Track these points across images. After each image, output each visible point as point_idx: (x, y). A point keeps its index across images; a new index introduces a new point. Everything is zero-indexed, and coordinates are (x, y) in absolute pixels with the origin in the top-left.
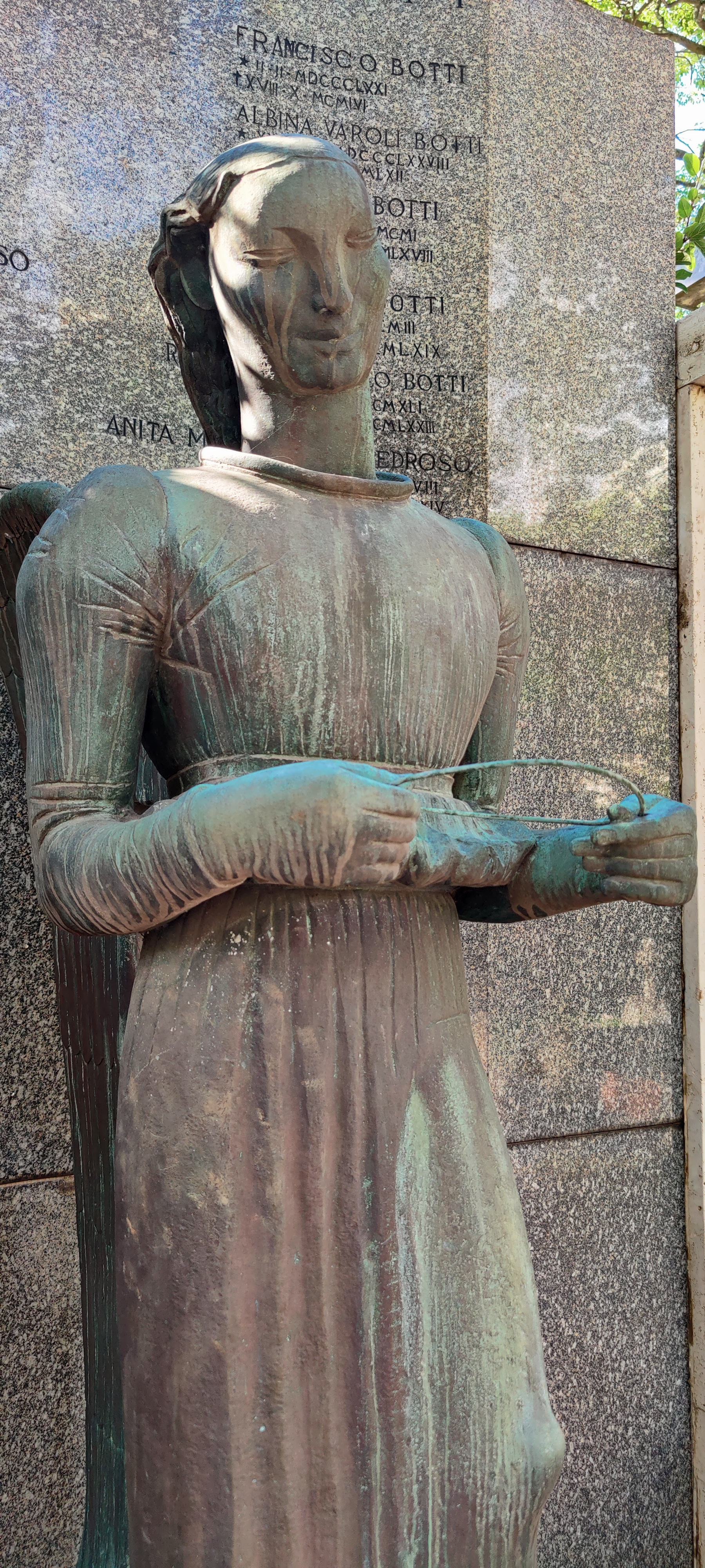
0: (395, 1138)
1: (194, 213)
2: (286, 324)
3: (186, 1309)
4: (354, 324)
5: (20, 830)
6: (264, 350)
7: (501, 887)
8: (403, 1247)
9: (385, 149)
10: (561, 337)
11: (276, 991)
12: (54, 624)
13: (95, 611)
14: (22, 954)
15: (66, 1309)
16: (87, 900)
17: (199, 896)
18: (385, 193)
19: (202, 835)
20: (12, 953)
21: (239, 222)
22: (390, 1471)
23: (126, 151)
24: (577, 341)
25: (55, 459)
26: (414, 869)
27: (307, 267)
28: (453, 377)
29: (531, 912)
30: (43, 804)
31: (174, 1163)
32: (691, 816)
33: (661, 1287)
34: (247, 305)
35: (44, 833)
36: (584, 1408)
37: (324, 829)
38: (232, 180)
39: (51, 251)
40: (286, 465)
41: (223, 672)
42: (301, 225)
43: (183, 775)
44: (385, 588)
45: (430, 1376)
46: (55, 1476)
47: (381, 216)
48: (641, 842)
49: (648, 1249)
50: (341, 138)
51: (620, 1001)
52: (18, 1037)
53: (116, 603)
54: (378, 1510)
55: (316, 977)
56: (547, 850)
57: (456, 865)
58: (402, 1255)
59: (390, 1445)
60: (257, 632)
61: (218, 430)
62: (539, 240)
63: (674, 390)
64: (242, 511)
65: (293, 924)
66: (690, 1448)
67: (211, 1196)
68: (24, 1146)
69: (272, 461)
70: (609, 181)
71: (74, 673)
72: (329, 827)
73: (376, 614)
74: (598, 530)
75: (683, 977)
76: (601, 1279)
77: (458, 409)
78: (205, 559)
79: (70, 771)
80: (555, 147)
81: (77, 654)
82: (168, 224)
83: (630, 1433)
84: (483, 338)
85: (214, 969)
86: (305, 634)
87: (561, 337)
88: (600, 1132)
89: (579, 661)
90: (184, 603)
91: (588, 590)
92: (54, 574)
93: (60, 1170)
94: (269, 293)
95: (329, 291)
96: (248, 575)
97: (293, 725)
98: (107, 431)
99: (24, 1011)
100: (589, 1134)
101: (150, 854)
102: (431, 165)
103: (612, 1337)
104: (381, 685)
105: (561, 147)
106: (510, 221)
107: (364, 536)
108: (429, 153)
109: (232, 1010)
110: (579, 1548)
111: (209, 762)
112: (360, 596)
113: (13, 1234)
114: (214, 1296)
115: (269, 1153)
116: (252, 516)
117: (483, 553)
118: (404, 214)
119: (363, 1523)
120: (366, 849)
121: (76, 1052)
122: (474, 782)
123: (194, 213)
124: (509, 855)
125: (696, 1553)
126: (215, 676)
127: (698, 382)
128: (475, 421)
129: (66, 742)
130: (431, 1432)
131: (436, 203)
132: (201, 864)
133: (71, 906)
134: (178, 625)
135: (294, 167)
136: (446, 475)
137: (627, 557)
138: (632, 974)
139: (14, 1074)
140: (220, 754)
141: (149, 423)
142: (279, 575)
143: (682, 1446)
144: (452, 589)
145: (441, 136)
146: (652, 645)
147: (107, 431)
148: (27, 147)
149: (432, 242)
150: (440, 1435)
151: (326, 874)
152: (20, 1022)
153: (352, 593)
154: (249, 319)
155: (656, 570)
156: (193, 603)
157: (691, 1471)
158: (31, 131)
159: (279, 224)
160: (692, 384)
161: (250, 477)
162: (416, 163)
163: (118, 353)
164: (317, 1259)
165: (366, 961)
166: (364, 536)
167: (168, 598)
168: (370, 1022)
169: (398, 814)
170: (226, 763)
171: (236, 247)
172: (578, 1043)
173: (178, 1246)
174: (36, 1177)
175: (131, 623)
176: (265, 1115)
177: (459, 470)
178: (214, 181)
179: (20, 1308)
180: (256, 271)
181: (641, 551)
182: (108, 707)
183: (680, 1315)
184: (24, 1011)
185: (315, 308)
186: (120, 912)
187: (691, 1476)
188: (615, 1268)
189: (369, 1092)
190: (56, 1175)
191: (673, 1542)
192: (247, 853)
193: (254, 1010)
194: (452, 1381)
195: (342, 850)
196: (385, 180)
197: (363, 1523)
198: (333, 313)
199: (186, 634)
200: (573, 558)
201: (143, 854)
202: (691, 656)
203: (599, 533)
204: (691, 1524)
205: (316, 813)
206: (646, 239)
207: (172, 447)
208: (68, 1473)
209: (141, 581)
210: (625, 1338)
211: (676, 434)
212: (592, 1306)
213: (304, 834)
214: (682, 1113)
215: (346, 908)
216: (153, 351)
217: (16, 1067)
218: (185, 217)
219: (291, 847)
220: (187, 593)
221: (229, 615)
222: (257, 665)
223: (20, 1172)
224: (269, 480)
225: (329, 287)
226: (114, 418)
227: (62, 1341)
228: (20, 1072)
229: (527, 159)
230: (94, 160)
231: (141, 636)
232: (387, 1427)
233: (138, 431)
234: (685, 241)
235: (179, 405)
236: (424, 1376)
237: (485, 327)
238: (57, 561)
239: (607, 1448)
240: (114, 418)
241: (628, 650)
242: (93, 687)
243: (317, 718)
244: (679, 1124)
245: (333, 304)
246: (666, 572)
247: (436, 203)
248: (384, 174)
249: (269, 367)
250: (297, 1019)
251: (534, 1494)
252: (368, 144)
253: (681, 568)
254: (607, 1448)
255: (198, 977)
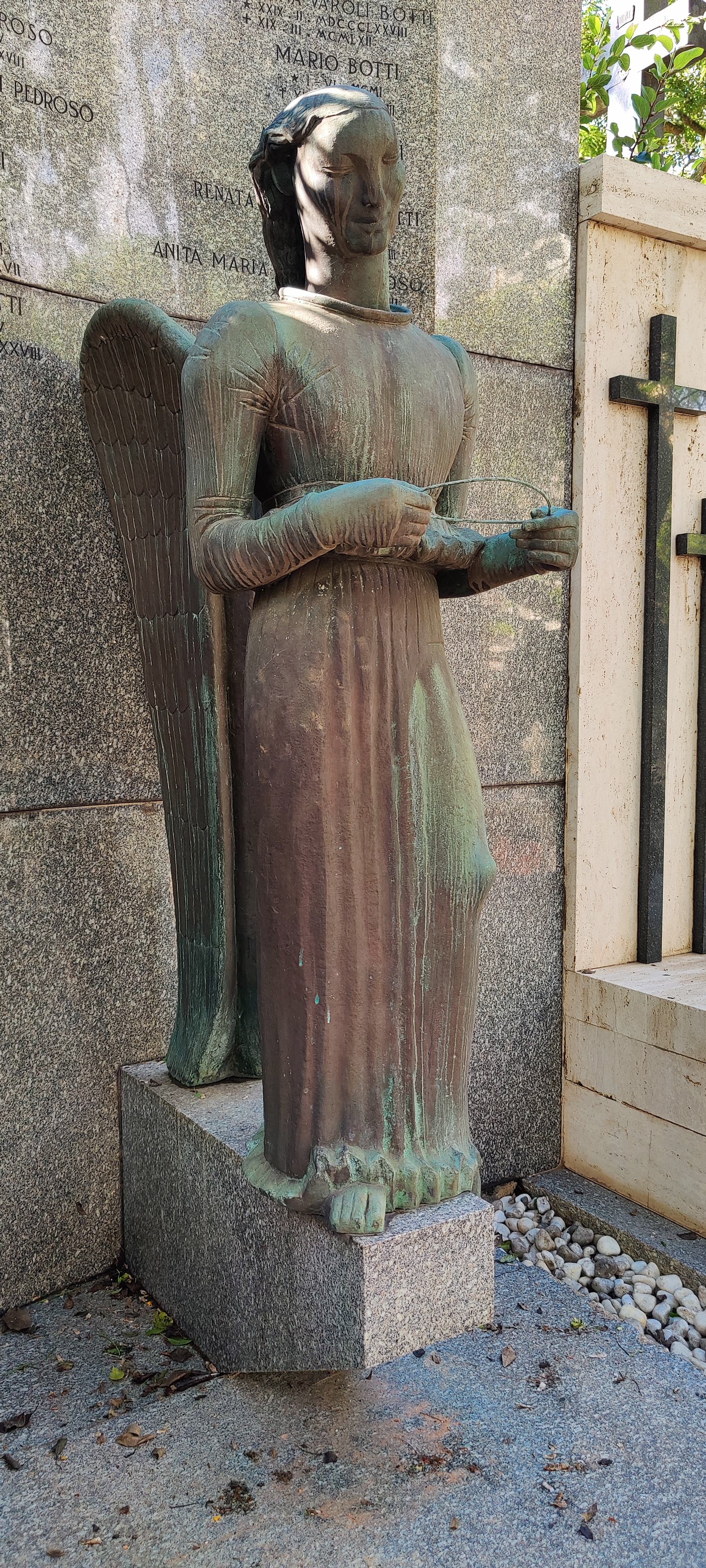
0: (408, 702)
1: (290, 138)
2: (345, 214)
3: (300, 786)
4: (385, 213)
5: (106, 558)
6: (330, 228)
7: (463, 570)
8: (412, 760)
9: (357, 18)
10: (491, 180)
11: (345, 616)
12: (213, 400)
13: (238, 392)
14: (112, 647)
15: (150, 889)
16: (238, 565)
17: (310, 555)
18: (358, 55)
19: (317, 519)
20: (105, 646)
21: (321, 149)
22: (406, 873)
23: (160, 20)
24: (503, 183)
25: (118, 276)
26: (420, 550)
27: (360, 177)
28: (410, 213)
29: (480, 586)
30: (204, 510)
31: (291, 709)
32: (577, 519)
33: (546, 892)
34: (323, 200)
35: (205, 528)
36: (492, 965)
37: (385, 514)
38: (316, 120)
39: (108, 105)
40: (342, 302)
41: (312, 431)
42: (358, 152)
43: (278, 497)
44: (402, 382)
45: (427, 827)
46: (148, 993)
47: (355, 75)
48: (549, 529)
49: (538, 866)
50: (323, 9)
51: (523, 695)
52: (112, 705)
53: (250, 388)
54: (400, 892)
55: (366, 609)
56: (492, 547)
57: (442, 550)
58: (412, 765)
59: (406, 860)
60: (333, 406)
61: (286, 274)
62: (475, 98)
63: (575, 224)
64: (319, 332)
65: (353, 579)
66: (561, 996)
67: (313, 725)
68: (119, 780)
69: (333, 299)
70: (530, 47)
71: (225, 430)
72: (388, 513)
73: (397, 397)
74: (515, 339)
75: (568, 679)
76: (505, 884)
77: (413, 240)
78: (301, 362)
79: (222, 490)
80: (488, 18)
81: (227, 418)
82: (268, 141)
83: (522, 983)
84: (433, 181)
85: (310, 604)
86: (359, 408)
87: (491, 180)
88: (507, 785)
89: (500, 441)
90: (287, 388)
91: (507, 387)
92: (214, 369)
93: (142, 798)
94: (338, 194)
95: (373, 193)
96: (326, 372)
97: (352, 463)
98: (154, 254)
99: (115, 687)
100: (499, 786)
101: (283, 532)
102: (393, 33)
103: (512, 922)
104: (400, 441)
105: (493, 19)
106: (454, 81)
107: (388, 348)
108: (391, 23)
109: (321, 626)
110: (487, 1053)
111: (299, 486)
112: (388, 386)
113: (114, 838)
114: (315, 777)
115: (344, 703)
116: (325, 335)
117: (454, 359)
118: (372, 74)
119: (392, 899)
120: (405, 526)
121: (162, 707)
122: (445, 508)
123: (290, 138)
124: (470, 549)
125: (564, 1063)
126: (306, 433)
127: (594, 218)
128: (426, 250)
129: (220, 472)
130: (427, 855)
131: (397, 65)
132: (315, 535)
133: (223, 570)
134: (283, 402)
135: (354, 115)
136: (404, 293)
137: (536, 361)
138: (532, 675)
139: (111, 730)
140: (307, 481)
141: (184, 248)
142: (343, 372)
143: (556, 995)
144: (438, 382)
145: (401, 9)
146: (554, 430)
147: (154, 254)
148: (88, 20)
149: (394, 98)
150: (432, 857)
151: (385, 539)
152: (112, 695)
153: (383, 384)
154: (323, 208)
155: (558, 372)
156: (294, 388)
157: (562, 1010)
158: (91, 7)
159: (345, 151)
160: (590, 219)
161: (319, 309)
162: (382, 30)
163: (159, 190)
164: (369, 764)
165: (392, 604)
166: (389, 348)
167: (278, 385)
168: (394, 637)
169: (422, 507)
170: (311, 486)
171: (318, 163)
172: (493, 723)
173: (295, 753)
174: (127, 801)
175: (257, 400)
176: (341, 683)
177: (414, 290)
178: (304, 120)
179: (121, 886)
180: (330, 179)
181: (546, 357)
182: (243, 451)
183: (558, 911)
184: (115, 687)
185: (364, 204)
186: (259, 570)
187: (562, 1014)
188: (515, 877)
189: (394, 676)
190: (140, 801)
191: (548, 1055)
192: (342, 528)
193: (334, 626)
194: (438, 830)
195: (394, 527)
196: (357, 44)
197: (392, 899)
198: (374, 207)
199: (288, 408)
200: (497, 361)
201: (277, 533)
202: (582, 440)
203: (516, 342)
204: (561, 1045)
205: (382, 505)
206: (557, 96)
207: (201, 268)
208: (157, 992)
209: (263, 375)
210: (520, 923)
211: (576, 261)
212: (499, 902)
213: (374, 517)
214: (564, 775)
215: (381, 572)
216: (184, 187)
217: (111, 725)
218: (282, 138)
219: (366, 525)
220: (290, 382)
221: (317, 396)
222: (333, 428)
223: (117, 797)
224: (331, 311)
225: (373, 190)
226: (158, 243)
227: (149, 909)
228: (114, 730)
229: (467, 29)
230: (137, 28)
231: (262, 409)
232: (404, 851)
233: (176, 254)
234: (588, 89)
235: (205, 233)
236: (424, 827)
237: (434, 171)
238: (215, 361)
239: (507, 992)
240: (158, 243)
241: (536, 434)
242: (235, 439)
243: (364, 460)
244: (562, 783)
245: (375, 202)
246: (565, 373)
247: (397, 65)
248: (356, 40)
249: (332, 239)
250: (357, 632)
251: (480, 889)
252: (344, 14)
253: (576, 370)
254: (507, 992)
255: (301, 608)
